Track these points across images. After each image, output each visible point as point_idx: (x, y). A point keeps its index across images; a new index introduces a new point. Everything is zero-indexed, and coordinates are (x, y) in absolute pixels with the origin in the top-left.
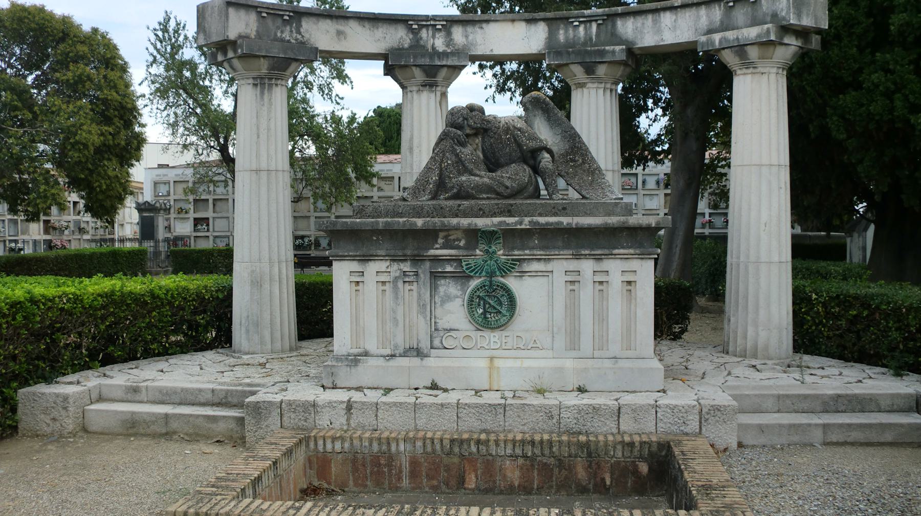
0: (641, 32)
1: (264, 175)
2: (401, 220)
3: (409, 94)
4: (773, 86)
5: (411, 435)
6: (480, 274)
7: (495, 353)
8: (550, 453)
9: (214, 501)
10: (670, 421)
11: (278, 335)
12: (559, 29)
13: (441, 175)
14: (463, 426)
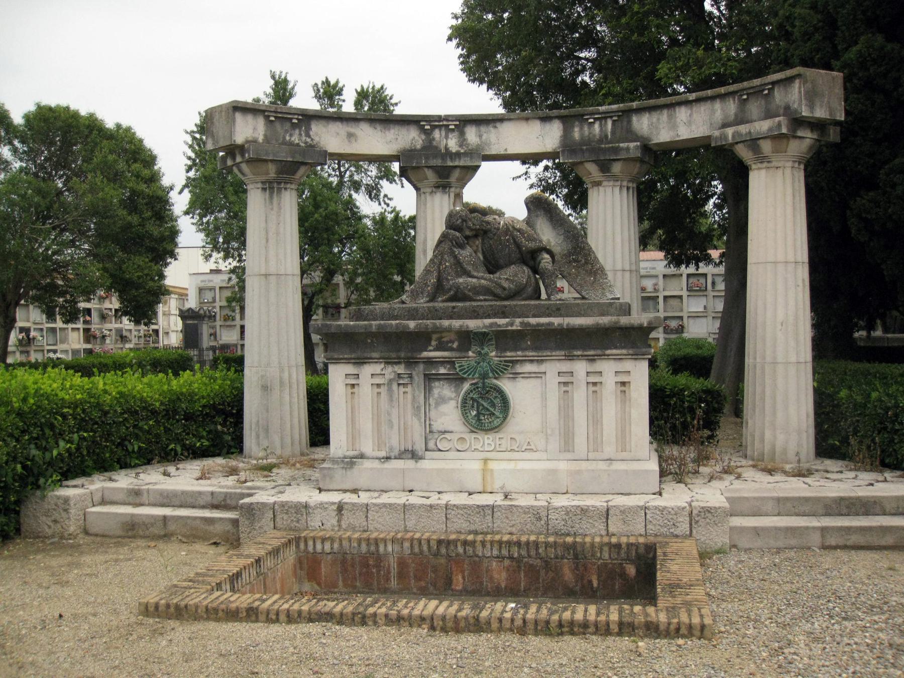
0: (657, 128)
1: (273, 279)
2: (394, 322)
3: (423, 196)
4: (789, 181)
5: (399, 536)
6: (468, 375)
7: (489, 455)
8: (536, 554)
9: (187, 593)
10: (660, 523)
11: (288, 440)
12: (573, 127)
13: (439, 279)
14: (453, 527)
